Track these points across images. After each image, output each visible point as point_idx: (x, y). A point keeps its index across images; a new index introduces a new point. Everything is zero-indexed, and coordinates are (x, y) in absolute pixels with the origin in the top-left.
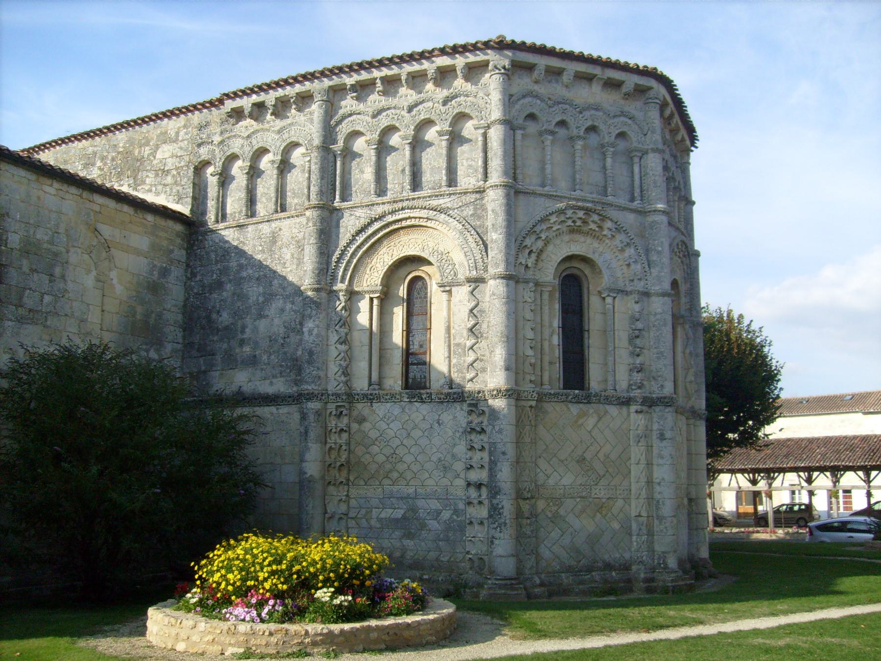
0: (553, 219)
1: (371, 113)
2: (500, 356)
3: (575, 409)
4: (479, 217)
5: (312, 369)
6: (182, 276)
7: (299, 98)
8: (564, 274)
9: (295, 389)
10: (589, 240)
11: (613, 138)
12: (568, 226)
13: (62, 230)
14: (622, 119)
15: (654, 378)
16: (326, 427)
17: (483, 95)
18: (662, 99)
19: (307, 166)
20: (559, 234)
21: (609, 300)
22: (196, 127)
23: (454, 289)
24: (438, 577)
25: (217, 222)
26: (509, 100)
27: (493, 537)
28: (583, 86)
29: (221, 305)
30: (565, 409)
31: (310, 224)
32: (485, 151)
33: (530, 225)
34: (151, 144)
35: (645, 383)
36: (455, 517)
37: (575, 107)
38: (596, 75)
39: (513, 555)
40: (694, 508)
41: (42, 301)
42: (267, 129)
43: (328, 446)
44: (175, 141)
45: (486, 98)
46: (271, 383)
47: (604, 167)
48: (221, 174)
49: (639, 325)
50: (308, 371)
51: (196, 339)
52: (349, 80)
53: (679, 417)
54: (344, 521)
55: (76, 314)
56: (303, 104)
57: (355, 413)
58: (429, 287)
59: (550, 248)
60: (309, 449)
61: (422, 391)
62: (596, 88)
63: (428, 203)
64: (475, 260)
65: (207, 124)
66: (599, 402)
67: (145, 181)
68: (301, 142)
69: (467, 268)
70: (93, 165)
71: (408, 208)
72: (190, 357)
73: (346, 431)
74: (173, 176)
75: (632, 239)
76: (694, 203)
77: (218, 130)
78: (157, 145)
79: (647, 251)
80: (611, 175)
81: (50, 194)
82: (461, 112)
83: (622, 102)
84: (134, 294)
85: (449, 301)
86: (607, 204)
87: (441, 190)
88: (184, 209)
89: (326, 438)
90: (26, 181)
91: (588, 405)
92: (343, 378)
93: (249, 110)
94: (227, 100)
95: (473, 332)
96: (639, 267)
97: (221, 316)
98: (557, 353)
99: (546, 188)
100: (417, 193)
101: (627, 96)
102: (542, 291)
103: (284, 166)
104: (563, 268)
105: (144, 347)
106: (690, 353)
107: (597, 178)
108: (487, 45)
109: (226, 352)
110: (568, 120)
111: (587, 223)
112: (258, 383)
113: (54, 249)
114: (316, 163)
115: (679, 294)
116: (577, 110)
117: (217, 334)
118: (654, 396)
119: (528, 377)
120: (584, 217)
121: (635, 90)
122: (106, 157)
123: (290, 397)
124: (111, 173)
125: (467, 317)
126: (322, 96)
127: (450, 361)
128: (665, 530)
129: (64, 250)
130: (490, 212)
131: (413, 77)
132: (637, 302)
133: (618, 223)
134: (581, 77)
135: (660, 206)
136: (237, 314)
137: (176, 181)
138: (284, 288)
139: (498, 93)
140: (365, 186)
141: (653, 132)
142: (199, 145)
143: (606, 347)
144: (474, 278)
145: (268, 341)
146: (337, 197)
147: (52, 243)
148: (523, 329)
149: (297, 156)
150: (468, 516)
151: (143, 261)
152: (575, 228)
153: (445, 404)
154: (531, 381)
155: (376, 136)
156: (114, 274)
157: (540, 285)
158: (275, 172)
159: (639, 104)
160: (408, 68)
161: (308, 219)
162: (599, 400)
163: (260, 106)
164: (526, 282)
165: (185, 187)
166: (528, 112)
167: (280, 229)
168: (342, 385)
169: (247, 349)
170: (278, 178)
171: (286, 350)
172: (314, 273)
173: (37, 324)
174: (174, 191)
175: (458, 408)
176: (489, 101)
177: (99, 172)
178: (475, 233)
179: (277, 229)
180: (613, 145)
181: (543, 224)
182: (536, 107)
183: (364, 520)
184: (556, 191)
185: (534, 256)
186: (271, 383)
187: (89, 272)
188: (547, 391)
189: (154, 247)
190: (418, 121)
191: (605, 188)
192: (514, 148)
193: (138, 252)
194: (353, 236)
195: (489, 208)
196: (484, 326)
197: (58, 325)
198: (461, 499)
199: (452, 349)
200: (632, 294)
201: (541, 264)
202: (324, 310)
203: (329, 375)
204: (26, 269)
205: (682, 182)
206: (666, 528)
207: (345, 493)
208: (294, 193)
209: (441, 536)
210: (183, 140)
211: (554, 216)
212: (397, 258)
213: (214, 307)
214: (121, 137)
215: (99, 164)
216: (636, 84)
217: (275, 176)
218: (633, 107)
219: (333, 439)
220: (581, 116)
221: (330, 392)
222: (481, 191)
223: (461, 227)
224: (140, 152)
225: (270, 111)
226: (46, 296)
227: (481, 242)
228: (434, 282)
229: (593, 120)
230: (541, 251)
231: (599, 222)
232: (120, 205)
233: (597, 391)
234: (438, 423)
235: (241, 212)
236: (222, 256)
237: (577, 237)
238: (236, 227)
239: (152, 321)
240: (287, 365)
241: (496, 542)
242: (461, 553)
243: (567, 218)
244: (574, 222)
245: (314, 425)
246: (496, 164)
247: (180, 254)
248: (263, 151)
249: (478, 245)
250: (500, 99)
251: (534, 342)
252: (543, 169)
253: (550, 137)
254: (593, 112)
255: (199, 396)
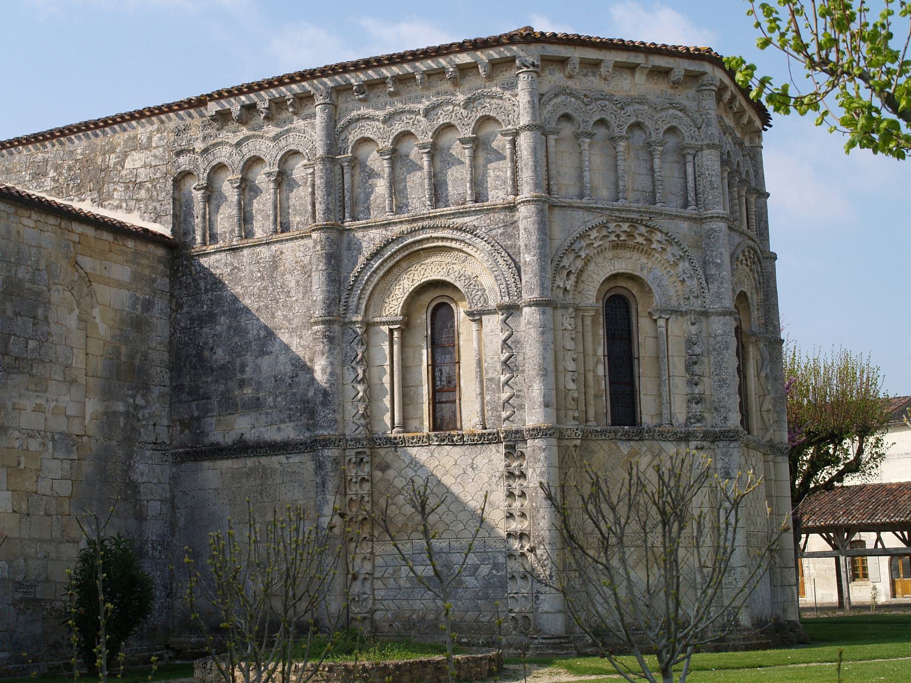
0: (594, 234)
1: (382, 118)
2: (539, 391)
3: (625, 448)
4: (510, 237)
5: (328, 411)
6: (166, 308)
7: (297, 100)
8: (608, 295)
9: (307, 434)
10: (636, 255)
11: (661, 135)
12: (610, 241)
13: (42, 266)
14: (671, 111)
15: (716, 409)
16: (345, 477)
17: (510, 96)
18: (718, 84)
19: (309, 179)
20: (601, 251)
21: (661, 322)
22: (173, 132)
23: (484, 317)
24: (478, 640)
25: (204, 243)
26: (539, 100)
27: (538, 592)
28: (625, 76)
29: (214, 341)
30: (614, 448)
31: (318, 248)
32: (514, 162)
33: (568, 243)
34: (118, 151)
35: (706, 415)
36: (495, 572)
37: (616, 102)
38: (640, 64)
39: (560, 612)
40: (778, 560)
41: (27, 347)
42: (259, 136)
43: (348, 497)
44: (148, 147)
45: (514, 99)
46: (279, 429)
47: (652, 169)
48: (206, 188)
49: (697, 350)
50: (322, 414)
51: (186, 381)
52: (355, 79)
53: (752, 452)
54: (369, 582)
55: (60, 360)
56: (301, 106)
57: (377, 460)
58: (456, 315)
59: (591, 267)
60: (327, 502)
61: (452, 433)
62: (640, 78)
63: (452, 221)
64: (507, 285)
65: (186, 128)
66: (653, 439)
67: (113, 195)
68: (301, 150)
69: (499, 294)
70: (45, 175)
71: (430, 228)
72: (179, 402)
73: (368, 480)
74: (148, 190)
75: (686, 252)
76: (768, 195)
77: (201, 135)
78: (126, 152)
79: (705, 263)
80: (659, 178)
81: (29, 227)
82: (485, 116)
83: (670, 91)
84: (118, 332)
85: (479, 331)
86: (656, 213)
87: (466, 206)
88: (164, 229)
89: (345, 489)
90: (5, 215)
91: (641, 443)
92: (362, 421)
93: (238, 113)
94: (210, 101)
95: (507, 365)
96: (695, 282)
97: (215, 353)
98: (604, 385)
99: (584, 200)
100: (438, 210)
101: (676, 84)
102: (583, 316)
103: (282, 179)
104: (607, 288)
105: (130, 392)
106: (766, 377)
107: (644, 182)
108: (511, 39)
109: (223, 394)
110: (608, 118)
111: (633, 236)
112: (262, 429)
113: (35, 288)
114: (321, 178)
115: (749, 308)
116: (618, 105)
117: (212, 374)
118: (716, 429)
119: (571, 413)
120: (628, 230)
121: (685, 76)
122: (61, 166)
123: (301, 444)
124: (68, 185)
125: (500, 349)
126: (324, 98)
127: (483, 398)
128: (734, 582)
129: (45, 288)
130: (522, 231)
131: (429, 75)
132: (693, 324)
133: (669, 235)
134: (620, 67)
135: (719, 210)
136: (235, 351)
137: (151, 197)
138: (289, 321)
139: (527, 94)
140: (378, 201)
141: (708, 124)
142: (179, 153)
143: (659, 376)
144: (506, 305)
145: (273, 381)
146: (347, 215)
147: (33, 281)
148: (564, 360)
149: (298, 171)
150: (509, 570)
151: (126, 294)
152: (619, 242)
153: (479, 446)
154: (574, 418)
155: (388, 144)
156: (96, 312)
157: (581, 310)
158: (272, 185)
159: (691, 92)
160: (421, 66)
161: (315, 242)
162: (653, 436)
163: (251, 108)
164: (565, 307)
165: (164, 203)
166: (562, 113)
167: (282, 253)
168: (361, 428)
169: (248, 391)
170: (275, 193)
171: (295, 390)
172: (325, 303)
173: (22, 373)
174: (150, 207)
175: (494, 450)
176: (517, 103)
177: (53, 183)
178: (506, 255)
179: (278, 253)
180: (661, 144)
181: (582, 241)
182: (571, 106)
183: (392, 580)
184: (596, 203)
185: (573, 278)
186: (279, 429)
187: (71, 311)
188: (593, 428)
189: (136, 277)
190: (437, 126)
191: (654, 193)
192: (547, 156)
193: (120, 285)
194: (367, 260)
195: (521, 227)
196: (520, 358)
197: (44, 373)
198: (501, 552)
199: (485, 384)
200: (687, 314)
201: (581, 286)
202: (339, 345)
203: (346, 418)
204: (9, 313)
205: (751, 171)
206: (735, 579)
207: (370, 550)
208: (295, 210)
209: (480, 594)
210: (157, 147)
211: (595, 231)
212: (419, 283)
213: (205, 344)
214: (79, 145)
215: (52, 174)
216: (686, 70)
217: (272, 191)
218: (686, 96)
219: (354, 490)
220: (623, 112)
221: (348, 438)
222: (511, 208)
223: (490, 248)
224: (103, 161)
225: (263, 116)
226: (30, 342)
227: (513, 265)
228: (462, 310)
229: (637, 116)
230: (581, 271)
231: (646, 234)
232: (99, 232)
233: (651, 426)
234: (472, 467)
235: (233, 231)
236: (212, 284)
237: (621, 252)
238: (229, 250)
239: (137, 362)
240: (297, 408)
241: (542, 597)
242: (503, 612)
243: (609, 232)
244: (618, 236)
245: (332, 474)
246: (526, 175)
247: (163, 283)
248: (256, 160)
249: (509, 268)
250: (529, 102)
251: (576, 374)
252: (581, 177)
253: (588, 140)
254: (637, 106)
255: (192, 447)
